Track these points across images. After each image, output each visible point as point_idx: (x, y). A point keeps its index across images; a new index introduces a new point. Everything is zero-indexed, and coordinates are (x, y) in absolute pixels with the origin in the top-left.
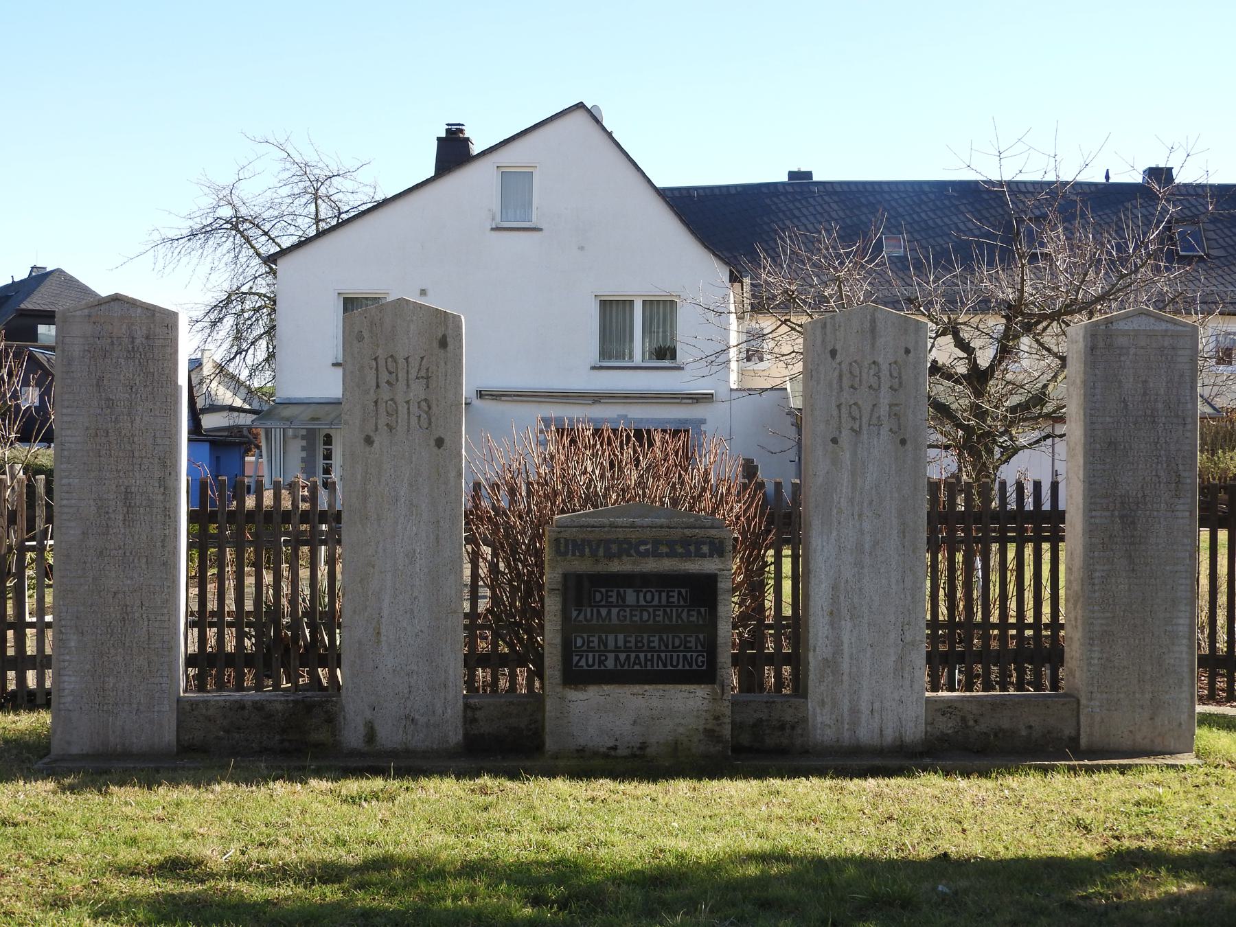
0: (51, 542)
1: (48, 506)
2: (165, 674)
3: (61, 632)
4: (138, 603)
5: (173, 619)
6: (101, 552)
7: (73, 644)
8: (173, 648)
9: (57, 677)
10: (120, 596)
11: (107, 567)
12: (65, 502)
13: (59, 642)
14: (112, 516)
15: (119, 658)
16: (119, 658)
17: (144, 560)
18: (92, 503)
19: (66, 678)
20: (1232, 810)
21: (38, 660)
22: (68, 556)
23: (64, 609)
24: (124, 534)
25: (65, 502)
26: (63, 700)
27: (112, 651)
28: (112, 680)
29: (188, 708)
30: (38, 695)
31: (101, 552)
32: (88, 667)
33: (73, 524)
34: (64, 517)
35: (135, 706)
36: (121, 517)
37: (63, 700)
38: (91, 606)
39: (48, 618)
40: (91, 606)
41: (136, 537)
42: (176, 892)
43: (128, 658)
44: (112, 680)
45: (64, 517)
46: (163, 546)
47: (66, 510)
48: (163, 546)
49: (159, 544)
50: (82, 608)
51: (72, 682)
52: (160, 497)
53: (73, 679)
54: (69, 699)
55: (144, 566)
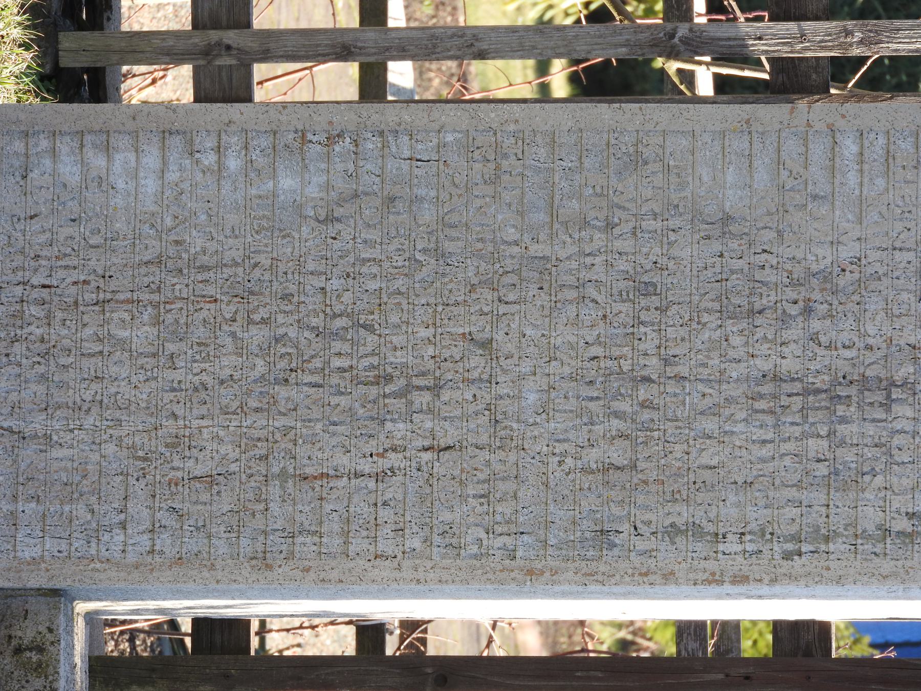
0: (705, 86)
1: (841, 68)
2: (164, 541)
3: (332, 139)
4: (449, 434)
5: (385, 569)
6: (649, 290)
7: (287, 182)
8: (267, 566)
9: (162, 123)
10: (477, 362)
11: (589, 313)
12: (850, 147)
13: (304, 129)
14: (794, 332)
15: (227, 363)
16: (227, 363)
17: (617, 454)
18: (846, 253)
19: (151, 160)
20: (5, 53)
21: (231, 37)
22: (637, 161)
23: (424, 149)
24: (722, 378)
25: (850, 147)
26: (65, 146)
27: (257, 336)
28: (142, 335)
29: (27, 633)
30: (90, 38)
31: (649, 290)
32: (196, 242)
33: (762, 177)
34: (791, 146)
35: (37, 424)
36: (789, 365)
37: (65, 146)
38: (439, 254)
39: (401, 74)
40: (439, 254)
41: (710, 425)
42: (76, 652)
43: (226, 396)
44: (142, 335)
45: (791, 146)
46: (673, 532)
47: (818, 149)
48: (673, 532)
49: (682, 514)
50: (428, 215)
51: (137, 179)
52: (870, 518)
53: (150, 185)
54: (69, 170)
55: (593, 456)
